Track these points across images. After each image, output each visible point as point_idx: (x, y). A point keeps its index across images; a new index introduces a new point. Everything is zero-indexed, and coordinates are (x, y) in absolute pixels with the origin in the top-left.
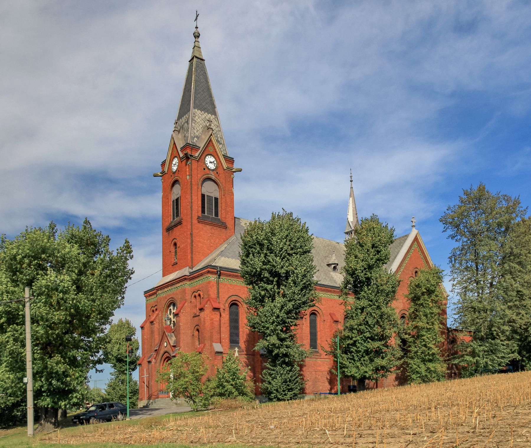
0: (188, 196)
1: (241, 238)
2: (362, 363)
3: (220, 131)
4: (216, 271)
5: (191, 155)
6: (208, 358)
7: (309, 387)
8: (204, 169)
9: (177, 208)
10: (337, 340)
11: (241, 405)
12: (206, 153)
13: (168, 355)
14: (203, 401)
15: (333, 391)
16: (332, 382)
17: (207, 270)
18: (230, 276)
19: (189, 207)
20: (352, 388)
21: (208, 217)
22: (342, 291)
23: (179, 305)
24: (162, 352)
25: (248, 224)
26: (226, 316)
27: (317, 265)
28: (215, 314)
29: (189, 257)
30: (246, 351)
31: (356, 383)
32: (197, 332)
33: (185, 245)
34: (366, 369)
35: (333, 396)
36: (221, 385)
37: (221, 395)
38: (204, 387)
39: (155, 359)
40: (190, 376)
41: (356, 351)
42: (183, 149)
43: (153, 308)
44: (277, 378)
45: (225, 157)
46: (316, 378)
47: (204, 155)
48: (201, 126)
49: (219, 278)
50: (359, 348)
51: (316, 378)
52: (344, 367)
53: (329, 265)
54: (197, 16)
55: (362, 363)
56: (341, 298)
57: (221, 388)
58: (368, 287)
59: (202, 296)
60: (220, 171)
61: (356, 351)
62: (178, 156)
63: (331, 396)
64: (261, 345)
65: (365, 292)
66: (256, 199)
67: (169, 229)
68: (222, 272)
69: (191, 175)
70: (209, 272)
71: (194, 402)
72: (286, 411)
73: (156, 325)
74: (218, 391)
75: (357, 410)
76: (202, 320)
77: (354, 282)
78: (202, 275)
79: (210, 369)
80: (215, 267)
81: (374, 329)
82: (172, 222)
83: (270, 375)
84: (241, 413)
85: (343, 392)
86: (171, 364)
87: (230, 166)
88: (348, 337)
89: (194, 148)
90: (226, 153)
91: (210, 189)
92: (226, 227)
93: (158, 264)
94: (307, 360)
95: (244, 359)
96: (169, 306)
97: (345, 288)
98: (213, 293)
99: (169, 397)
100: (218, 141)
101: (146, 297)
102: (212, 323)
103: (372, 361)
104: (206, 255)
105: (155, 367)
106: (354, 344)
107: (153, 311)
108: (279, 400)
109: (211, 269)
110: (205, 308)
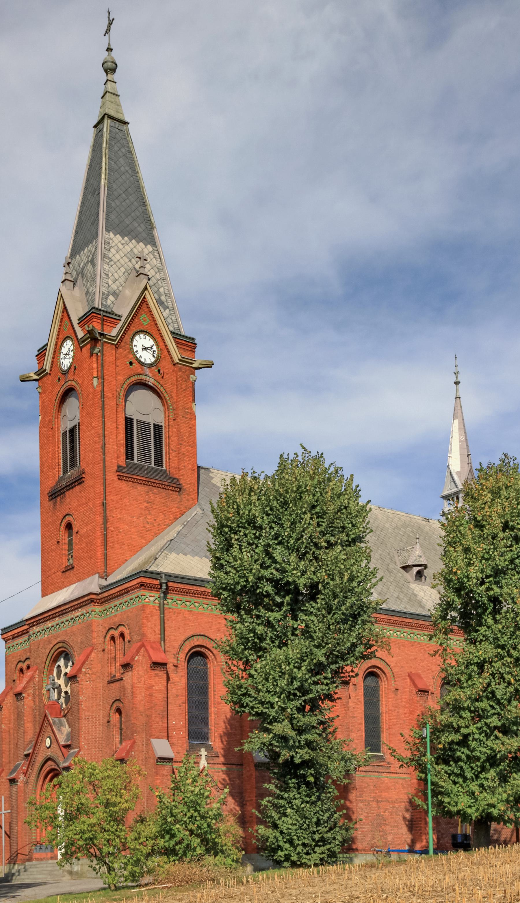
0: (97, 423)
1: (213, 512)
2: (482, 786)
3: (164, 279)
4: (158, 582)
5: (101, 334)
6: (139, 772)
7: (362, 833)
8: (131, 363)
9: (73, 449)
10: (426, 732)
11: (213, 875)
12: (133, 329)
13: (54, 766)
14: (130, 867)
15: (418, 847)
16: (414, 825)
17: (139, 580)
18: (187, 593)
19: (99, 446)
20: (459, 840)
21: (140, 468)
22: (435, 624)
23: (78, 657)
24: (40, 759)
25: (228, 482)
26: (179, 680)
27: (378, 566)
28: (157, 675)
29: (100, 554)
30: (224, 756)
31: (469, 830)
32: (117, 715)
33: (89, 527)
34: (493, 800)
35: (417, 856)
36: (166, 832)
37: (169, 852)
38: (131, 836)
39: (25, 774)
40: (101, 813)
41: (468, 756)
42: (83, 321)
43: (21, 664)
44: (291, 814)
45: (176, 336)
46: (378, 815)
47: (130, 333)
48: (123, 270)
49: (165, 598)
50: (474, 750)
51: (378, 815)
52: (441, 793)
53: (406, 568)
54: (110, 24)
55: (482, 786)
56: (434, 639)
57: (167, 837)
58: (494, 619)
59: (127, 637)
60: (165, 366)
61: (468, 756)
62: (73, 336)
63: (411, 858)
64: (256, 744)
65: (488, 627)
66: (243, 428)
67: (55, 495)
68: (170, 584)
69: (102, 377)
70: (142, 585)
71: (110, 869)
72: (311, 889)
73: (28, 702)
74: (161, 842)
75: (472, 893)
76: (129, 688)
77: (465, 605)
78: (127, 591)
79: (146, 795)
80: (156, 575)
81: (509, 708)
82: (61, 479)
83: (275, 806)
84: (213, 892)
85: (440, 849)
86: (60, 784)
87: (187, 355)
88: (450, 726)
89: (109, 317)
90: (179, 329)
91: (144, 407)
92: (179, 489)
93: (32, 570)
94: (358, 775)
95: (219, 773)
96: (56, 660)
97: (444, 618)
98: (152, 632)
99: (56, 857)
100: (160, 302)
101: (6, 640)
102: (151, 695)
103: (504, 779)
104: (135, 550)
105: (25, 793)
106: (464, 742)
107: (21, 670)
108: (294, 865)
109: (149, 580)
110: (134, 664)
